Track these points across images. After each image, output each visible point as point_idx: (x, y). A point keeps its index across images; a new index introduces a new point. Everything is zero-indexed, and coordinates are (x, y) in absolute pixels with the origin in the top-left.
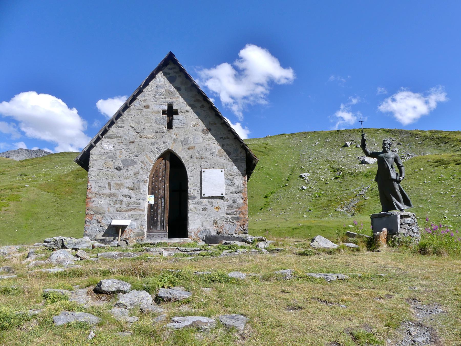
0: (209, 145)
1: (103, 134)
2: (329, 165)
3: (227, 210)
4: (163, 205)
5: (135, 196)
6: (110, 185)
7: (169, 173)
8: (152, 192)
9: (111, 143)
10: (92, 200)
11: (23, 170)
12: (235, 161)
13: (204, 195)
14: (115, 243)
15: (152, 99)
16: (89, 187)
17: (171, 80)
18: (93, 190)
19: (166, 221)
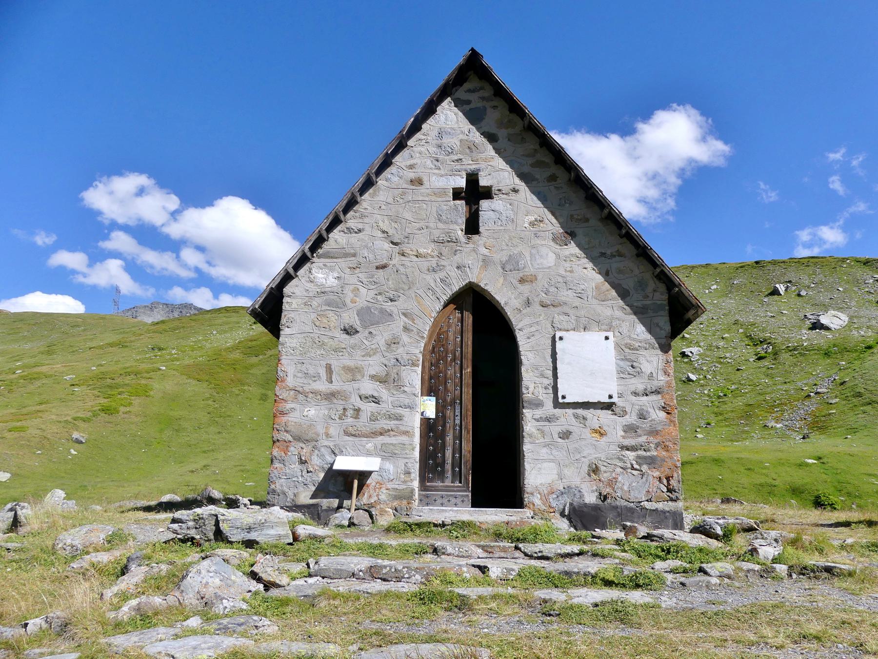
0: (571, 272)
1: (314, 248)
2: (741, 331)
3: (624, 437)
4: (458, 422)
5: (390, 399)
6: (329, 369)
7: (470, 343)
8: (430, 389)
9: (332, 269)
10: (289, 406)
11: (159, 340)
12: (640, 312)
13: (564, 397)
14: (343, 517)
15: (429, 162)
16: (281, 374)
17: (474, 117)
18: (290, 381)
19: (466, 463)
